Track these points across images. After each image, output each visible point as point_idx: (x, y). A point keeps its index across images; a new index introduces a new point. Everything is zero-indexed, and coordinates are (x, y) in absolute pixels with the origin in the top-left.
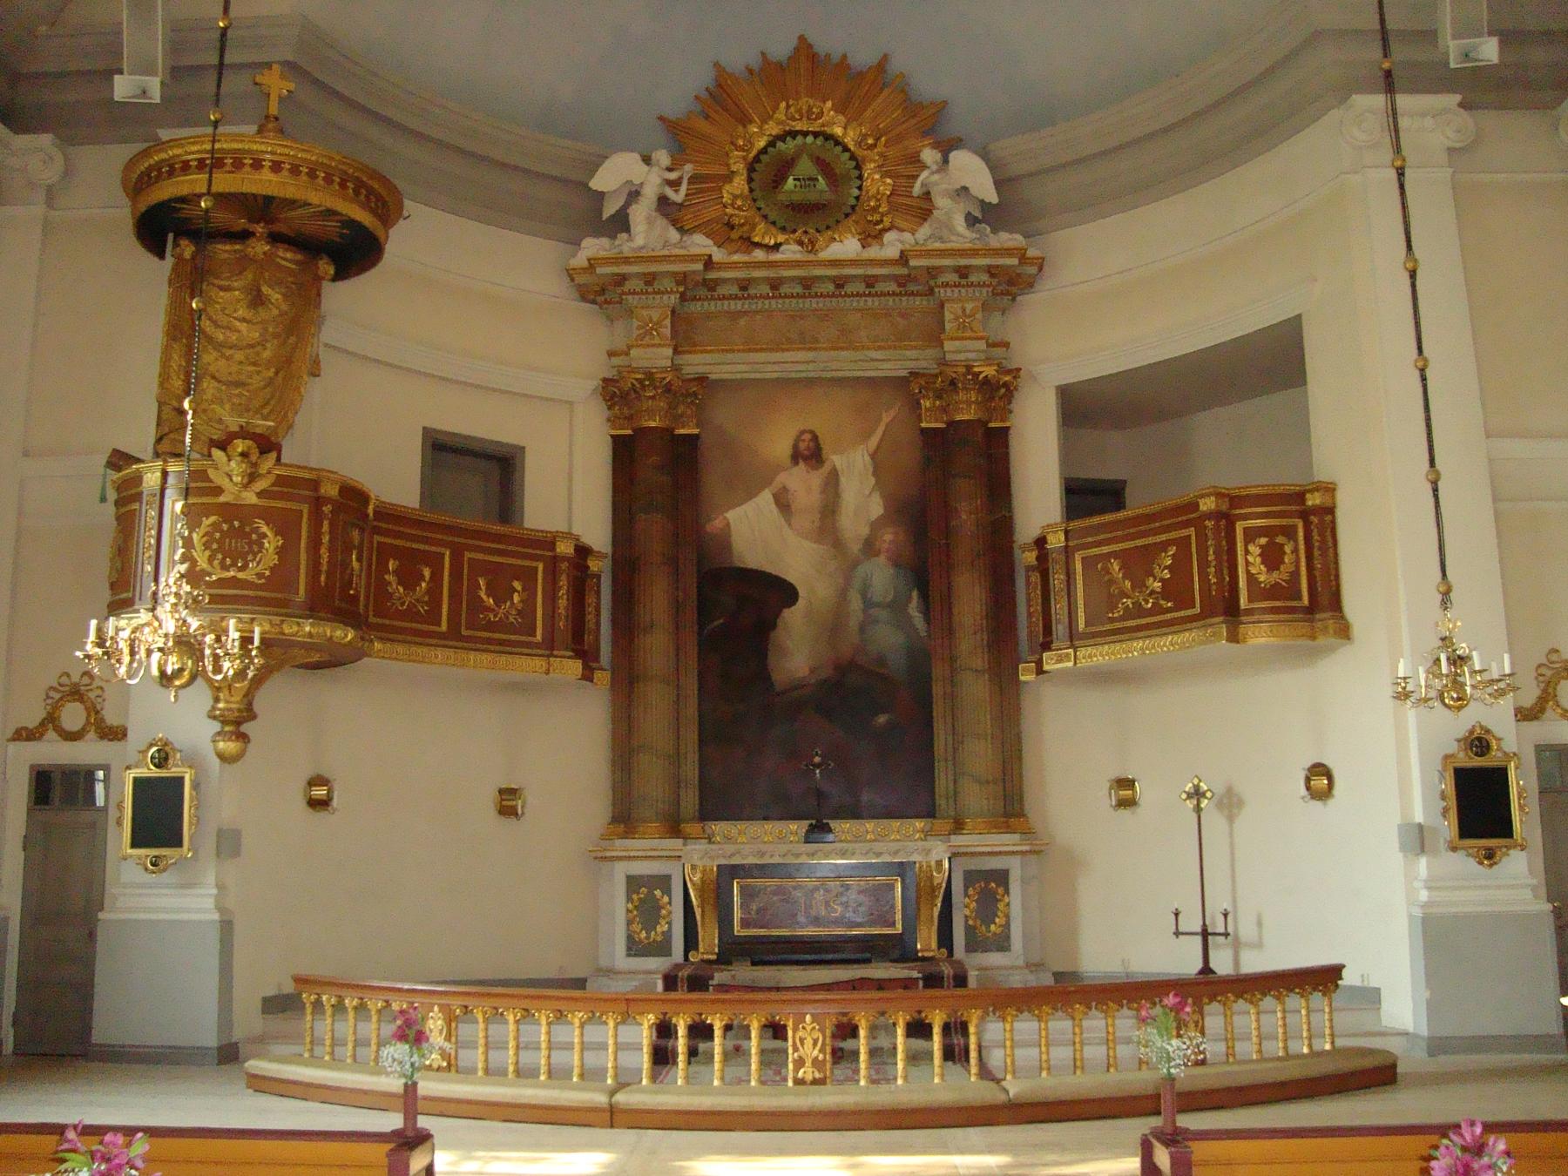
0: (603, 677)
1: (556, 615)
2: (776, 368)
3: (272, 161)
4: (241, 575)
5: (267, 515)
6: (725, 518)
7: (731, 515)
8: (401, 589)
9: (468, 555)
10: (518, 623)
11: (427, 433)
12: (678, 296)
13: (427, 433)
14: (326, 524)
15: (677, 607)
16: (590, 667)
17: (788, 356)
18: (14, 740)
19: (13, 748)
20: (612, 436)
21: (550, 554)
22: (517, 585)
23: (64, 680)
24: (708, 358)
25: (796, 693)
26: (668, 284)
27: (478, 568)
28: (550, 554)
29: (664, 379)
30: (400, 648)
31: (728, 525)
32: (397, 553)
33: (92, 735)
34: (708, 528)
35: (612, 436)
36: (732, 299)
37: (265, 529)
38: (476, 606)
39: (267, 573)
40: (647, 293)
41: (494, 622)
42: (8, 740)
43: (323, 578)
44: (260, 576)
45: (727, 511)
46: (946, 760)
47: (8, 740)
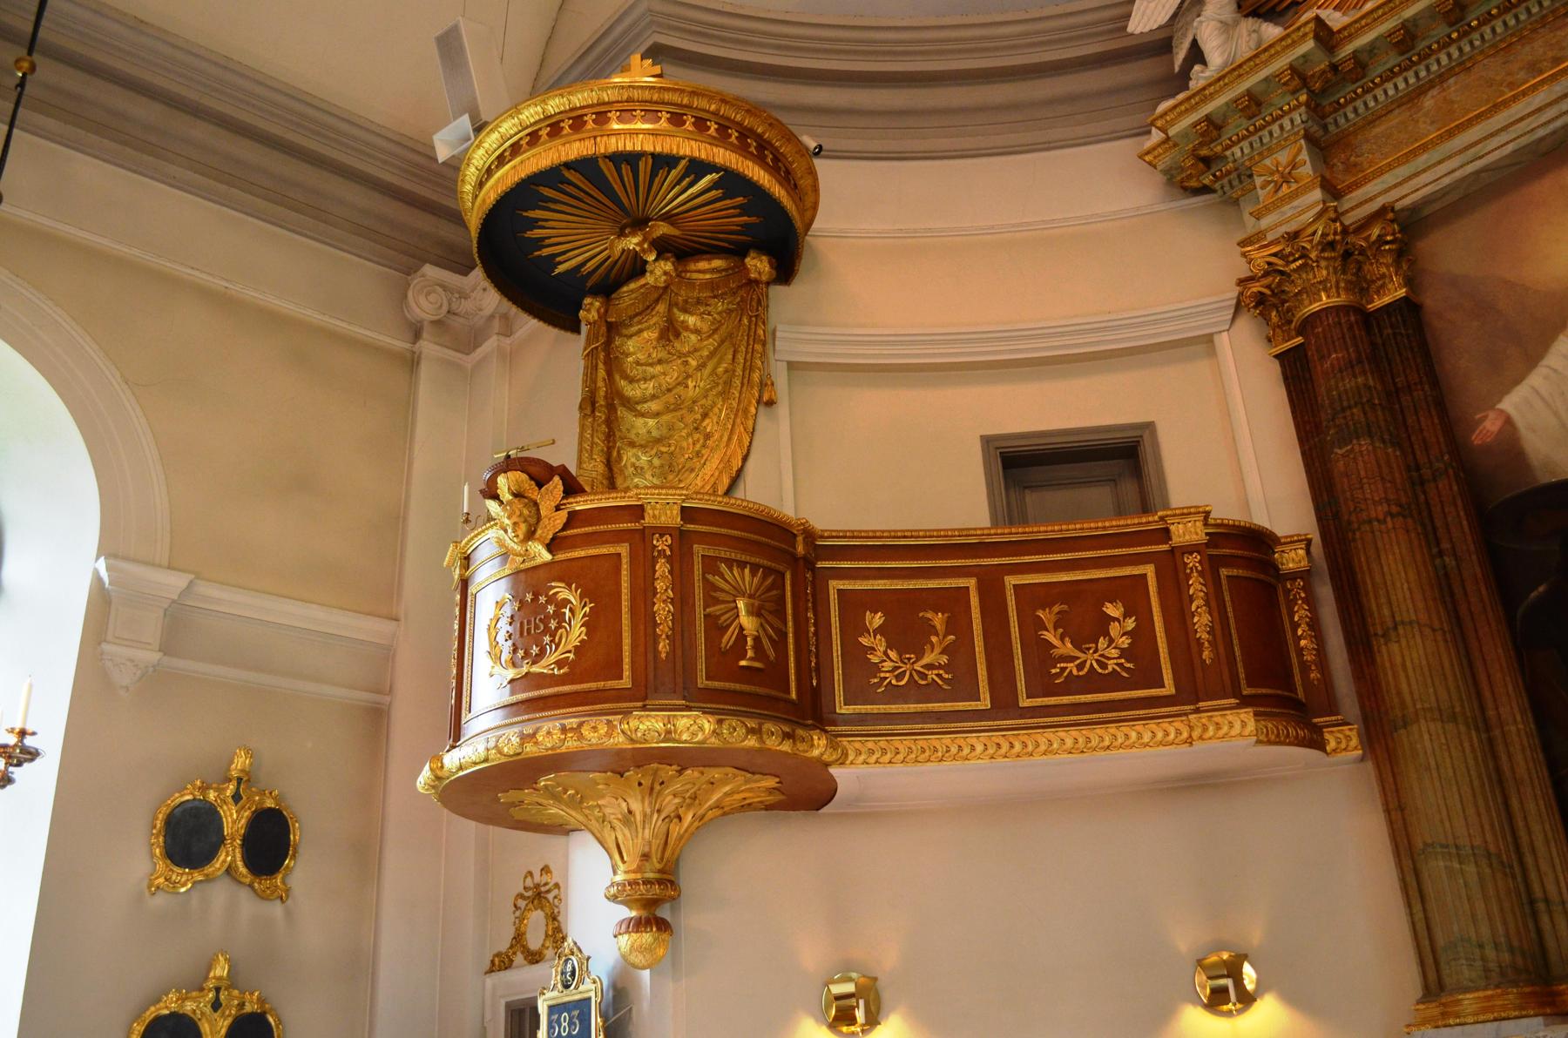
0: (1345, 741)
1: (1193, 644)
2: (1503, 138)
3: (548, 126)
4: (536, 669)
5: (566, 574)
6: (1502, 411)
7: (1510, 404)
8: (893, 654)
9: (1011, 581)
10: (1127, 670)
11: (987, 441)
12: (1303, 109)
13: (987, 441)
14: (662, 568)
15: (1445, 589)
16: (1315, 725)
17: (1518, 109)
18: (491, 971)
19: (490, 981)
20: (1276, 357)
21: (1165, 547)
22: (1113, 610)
23: (529, 882)
24: (1389, 179)
25: (589, 264)
26: (1282, 100)
27: (1032, 598)
28: (1165, 547)
29: (1314, 233)
30: (902, 744)
31: (1509, 421)
32: (874, 601)
33: (519, 958)
34: (1476, 439)
35: (1276, 357)
36: (1396, 75)
37: (564, 594)
38: (1040, 655)
39: (571, 656)
40: (1257, 130)
41: (1078, 676)
42: (486, 973)
43: (663, 646)
44: (560, 664)
45: (1500, 401)
46: (1164, 7)
47: (486, 973)
